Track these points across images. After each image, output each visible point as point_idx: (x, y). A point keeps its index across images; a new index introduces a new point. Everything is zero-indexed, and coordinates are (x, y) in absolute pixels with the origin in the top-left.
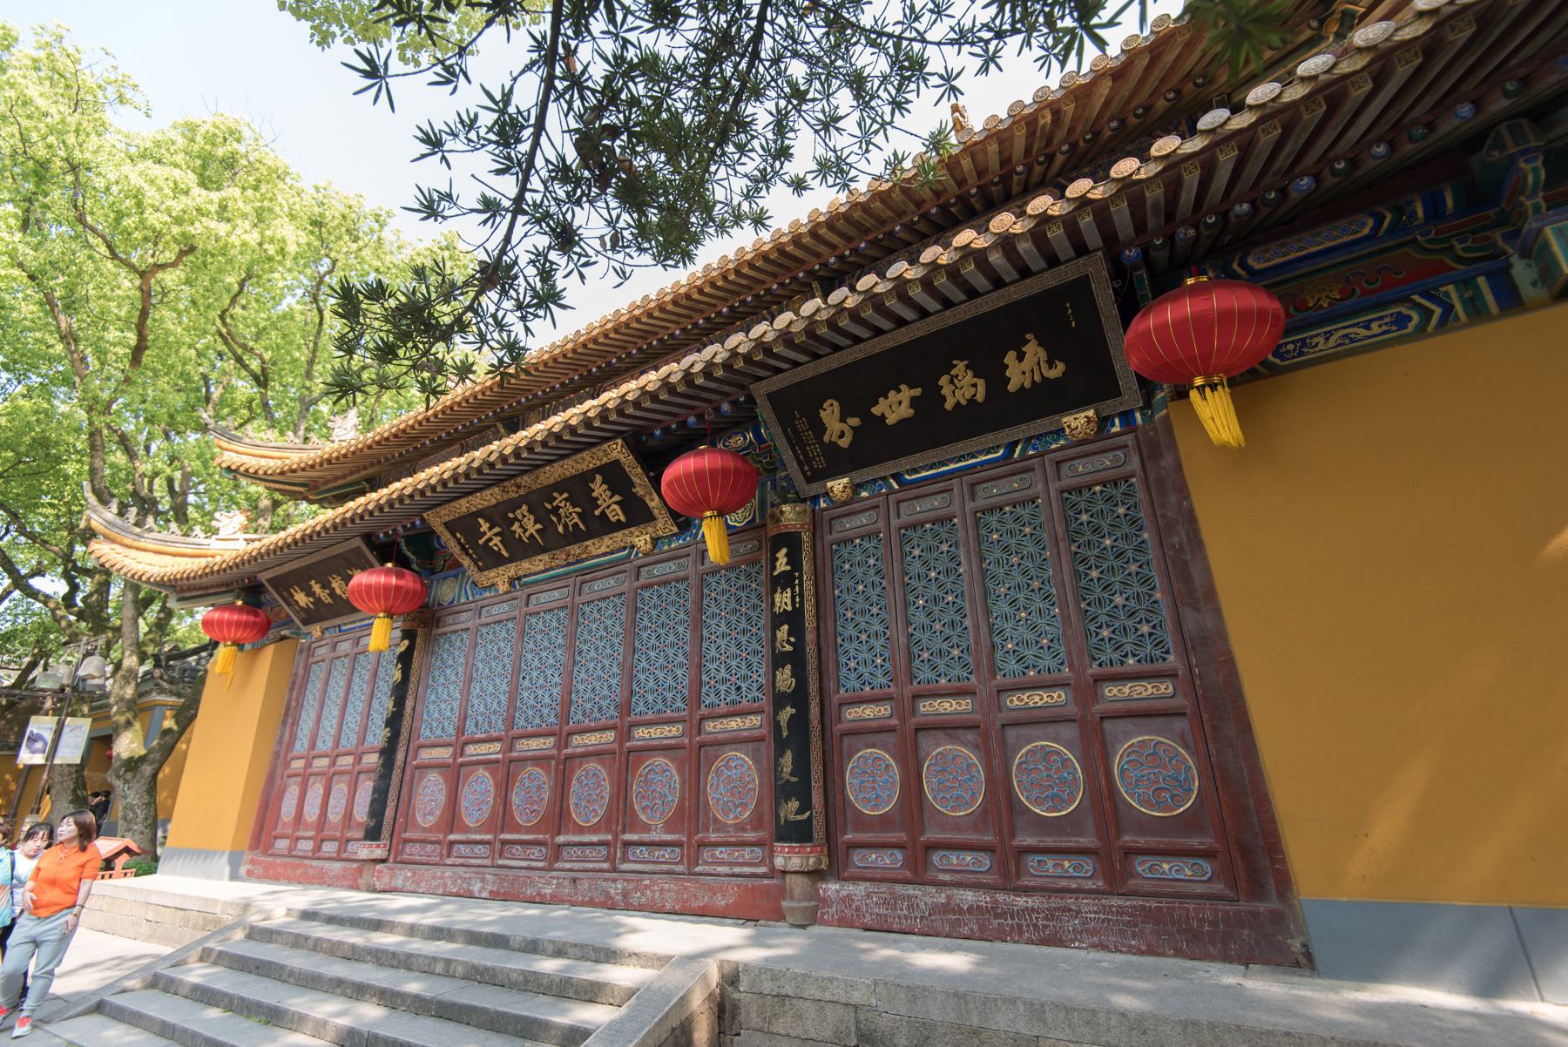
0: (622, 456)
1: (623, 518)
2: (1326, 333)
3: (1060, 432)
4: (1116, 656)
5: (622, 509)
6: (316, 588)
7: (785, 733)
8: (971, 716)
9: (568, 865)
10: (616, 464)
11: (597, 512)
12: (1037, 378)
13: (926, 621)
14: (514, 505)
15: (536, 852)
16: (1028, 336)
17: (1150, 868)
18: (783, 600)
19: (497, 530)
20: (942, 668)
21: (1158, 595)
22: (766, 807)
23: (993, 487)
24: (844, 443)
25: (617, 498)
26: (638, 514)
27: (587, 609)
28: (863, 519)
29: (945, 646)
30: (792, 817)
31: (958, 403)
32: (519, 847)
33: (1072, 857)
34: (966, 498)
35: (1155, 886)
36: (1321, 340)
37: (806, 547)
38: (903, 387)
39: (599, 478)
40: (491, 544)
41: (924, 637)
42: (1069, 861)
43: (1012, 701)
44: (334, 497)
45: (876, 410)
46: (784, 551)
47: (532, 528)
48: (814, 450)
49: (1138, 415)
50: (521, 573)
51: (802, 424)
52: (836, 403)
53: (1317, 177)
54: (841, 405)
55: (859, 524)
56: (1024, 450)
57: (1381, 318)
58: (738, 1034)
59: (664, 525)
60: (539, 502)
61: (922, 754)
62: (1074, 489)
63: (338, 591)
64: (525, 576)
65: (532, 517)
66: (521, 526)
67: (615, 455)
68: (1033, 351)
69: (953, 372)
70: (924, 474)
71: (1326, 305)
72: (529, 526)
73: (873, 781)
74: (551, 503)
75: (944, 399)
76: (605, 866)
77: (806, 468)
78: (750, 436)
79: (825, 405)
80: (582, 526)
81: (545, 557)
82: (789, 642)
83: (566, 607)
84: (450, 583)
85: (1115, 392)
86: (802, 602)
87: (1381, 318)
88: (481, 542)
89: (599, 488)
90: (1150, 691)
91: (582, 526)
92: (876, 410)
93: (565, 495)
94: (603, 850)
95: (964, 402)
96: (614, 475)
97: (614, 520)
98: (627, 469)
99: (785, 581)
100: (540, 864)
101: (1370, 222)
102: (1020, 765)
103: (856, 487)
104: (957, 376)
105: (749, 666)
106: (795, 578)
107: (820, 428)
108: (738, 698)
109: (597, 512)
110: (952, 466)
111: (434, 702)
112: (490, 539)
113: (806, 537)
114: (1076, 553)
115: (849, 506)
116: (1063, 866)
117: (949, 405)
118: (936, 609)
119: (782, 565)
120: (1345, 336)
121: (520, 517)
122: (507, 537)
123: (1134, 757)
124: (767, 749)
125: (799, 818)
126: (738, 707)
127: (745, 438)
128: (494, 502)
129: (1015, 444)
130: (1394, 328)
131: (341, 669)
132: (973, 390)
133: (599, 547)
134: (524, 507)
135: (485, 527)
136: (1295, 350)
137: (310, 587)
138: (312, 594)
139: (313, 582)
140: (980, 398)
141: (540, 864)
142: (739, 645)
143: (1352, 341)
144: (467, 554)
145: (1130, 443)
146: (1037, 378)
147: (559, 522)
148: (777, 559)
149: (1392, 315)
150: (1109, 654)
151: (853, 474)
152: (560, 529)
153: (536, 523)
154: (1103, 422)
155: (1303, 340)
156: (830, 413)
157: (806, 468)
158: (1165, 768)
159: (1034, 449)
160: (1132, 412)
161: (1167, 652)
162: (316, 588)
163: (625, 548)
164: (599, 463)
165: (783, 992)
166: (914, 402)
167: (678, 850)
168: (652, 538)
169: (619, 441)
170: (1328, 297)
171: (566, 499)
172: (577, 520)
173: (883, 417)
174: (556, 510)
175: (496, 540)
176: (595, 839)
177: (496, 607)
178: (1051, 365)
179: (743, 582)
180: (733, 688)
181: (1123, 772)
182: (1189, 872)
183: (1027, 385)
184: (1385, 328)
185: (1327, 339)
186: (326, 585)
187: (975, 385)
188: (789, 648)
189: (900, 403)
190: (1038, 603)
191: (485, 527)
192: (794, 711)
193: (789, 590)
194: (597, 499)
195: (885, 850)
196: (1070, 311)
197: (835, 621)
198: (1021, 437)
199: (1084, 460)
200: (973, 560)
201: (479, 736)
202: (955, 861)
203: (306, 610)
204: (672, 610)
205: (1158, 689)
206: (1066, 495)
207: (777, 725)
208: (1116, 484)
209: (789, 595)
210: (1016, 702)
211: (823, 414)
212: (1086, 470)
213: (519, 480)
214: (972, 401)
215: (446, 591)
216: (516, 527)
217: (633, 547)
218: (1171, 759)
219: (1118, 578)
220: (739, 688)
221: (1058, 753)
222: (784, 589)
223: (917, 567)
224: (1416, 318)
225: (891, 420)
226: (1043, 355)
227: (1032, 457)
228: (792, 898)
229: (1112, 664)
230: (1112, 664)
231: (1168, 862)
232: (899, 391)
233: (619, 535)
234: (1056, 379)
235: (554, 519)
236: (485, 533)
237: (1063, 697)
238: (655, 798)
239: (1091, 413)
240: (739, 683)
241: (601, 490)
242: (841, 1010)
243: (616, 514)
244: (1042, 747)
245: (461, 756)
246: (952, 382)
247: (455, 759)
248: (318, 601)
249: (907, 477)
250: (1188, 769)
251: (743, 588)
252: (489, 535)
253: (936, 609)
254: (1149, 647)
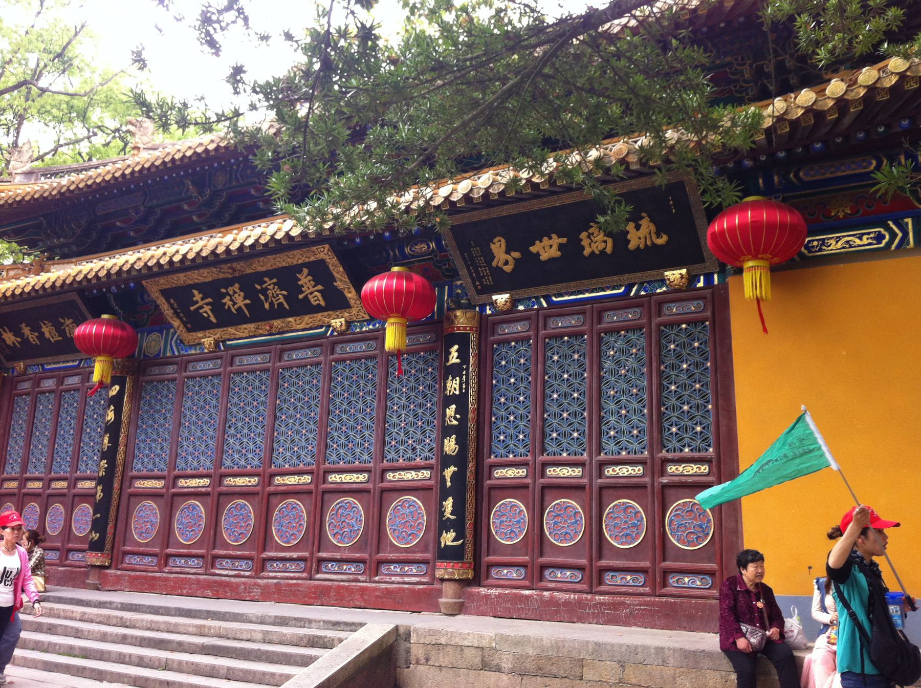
0: (327, 257)
1: (322, 303)
2: (837, 237)
3: (663, 281)
4: (678, 445)
5: (323, 296)
6: (26, 331)
7: (449, 484)
8: (581, 480)
9: (271, 574)
10: (322, 262)
11: (301, 297)
12: (649, 243)
13: (557, 410)
14: (228, 283)
15: (243, 564)
16: (643, 214)
17: (678, 580)
18: (453, 386)
19: (209, 300)
20: (565, 445)
21: (710, 407)
22: (432, 535)
23: (614, 315)
24: (508, 269)
25: (320, 287)
26: (336, 302)
27: (287, 374)
28: (519, 327)
29: (568, 429)
30: (449, 543)
31: (593, 252)
32: (229, 561)
33: (632, 573)
34: (595, 321)
35: (677, 591)
36: (833, 242)
37: (473, 345)
38: (554, 236)
39: (305, 271)
40: (201, 311)
41: (555, 422)
42: (631, 576)
43: (608, 471)
44: (13, 230)
45: (533, 249)
46: (456, 347)
47: (241, 301)
48: (484, 271)
49: (716, 276)
50: (225, 337)
51: (476, 251)
52: (503, 240)
53: (825, 142)
54: (506, 242)
55: (515, 330)
56: (638, 291)
57: (869, 234)
58: (409, 667)
59: (357, 311)
60: (249, 284)
61: (546, 504)
62: (669, 325)
63: (47, 335)
64: (229, 340)
65: (242, 294)
66: (231, 300)
67: (321, 256)
68: (647, 225)
69: (590, 231)
70: (566, 298)
71: (841, 217)
72: (237, 300)
73: (510, 521)
74: (261, 285)
75: (583, 248)
76: (304, 575)
77: (477, 283)
78: (433, 245)
79: (495, 240)
80: (286, 306)
81: (251, 326)
82: (455, 418)
83: (268, 370)
84: (154, 336)
85: (702, 260)
86: (467, 389)
87: (869, 234)
88: (192, 308)
89: (305, 280)
90: (694, 471)
91: (286, 306)
92: (533, 249)
93: (275, 280)
94: (302, 565)
95: (597, 252)
96: (319, 272)
97: (315, 303)
98: (331, 268)
99: (455, 371)
100: (247, 574)
101: (874, 163)
102: (609, 514)
103: (514, 302)
104: (593, 234)
105: (423, 432)
106: (463, 369)
107: (490, 256)
108: (414, 456)
109: (301, 297)
110: (587, 295)
111: (144, 441)
112: (202, 307)
113: (472, 337)
114: (664, 372)
115: (509, 315)
116: (626, 579)
117: (587, 252)
118: (565, 402)
119: (454, 358)
120: (848, 242)
121: (231, 293)
122: (218, 307)
123: (678, 512)
124: (434, 495)
125: (455, 543)
126: (413, 463)
127: (429, 247)
128: (210, 279)
129: (633, 285)
130: (875, 242)
131: (46, 406)
132: (603, 245)
133: (299, 326)
134: (237, 285)
135: (197, 296)
136: (817, 246)
137: (21, 329)
138: (21, 335)
139: (23, 325)
140: (609, 250)
141: (247, 574)
142: (416, 415)
143: (851, 246)
144: (178, 317)
145: (708, 296)
146: (649, 243)
147: (266, 300)
148: (450, 353)
149: (875, 232)
150: (674, 443)
151: (513, 292)
152: (267, 306)
153: (245, 298)
154: (692, 279)
155: (823, 240)
156: (498, 248)
157: (477, 283)
158: (696, 520)
159: (645, 291)
160: (712, 274)
161: (709, 446)
162: (26, 331)
163: (321, 327)
164: (307, 260)
165: (439, 642)
166: (561, 247)
167: (362, 565)
168: (346, 321)
169: (327, 246)
170: (843, 211)
171: (275, 284)
172: (282, 300)
173: (538, 254)
174: (264, 291)
175: (207, 308)
176: (295, 555)
177: (201, 364)
178: (658, 236)
179: (421, 365)
180: (410, 448)
181: (671, 522)
182: (698, 583)
183: (642, 246)
184: (870, 241)
185: (837, 242)
186: (36, 328)
187: (605, 242)
188: (455, 423)
189: (551, 246)
190: (635, 405)
191: (197, 296)
192: (456, 469)
193: (458, 378)
194: (302, 286)
195: (513, 568)
196: (671, 203)
197: (492, 404)
198: (637, 281)
199: (678, 304)
200: (538, 411)
201: (189, 471)
202: (559, 575)
203: (13, 348)
204: (362, 383)
205: (700, 468)
206: (662, 328)
207: (443, 479)
208: (696, 325)
209: (458, 382)
210: (611, 472)
211: (492, 246)
212: (678, 312)
213: (235, 265)
214: (603, 252)
215: (152, 343)
216: (226, 300)
217: (329, 326)
218: (700, 515)
219: (687, 393)
220: (414, 449)
221: (633, 508)
222: (454, 378)
223: (555, 370)
224: (887, 237)
225: (544, 257)
226: (653, 228)
227: (643, 296)
228: (447, 597)
229: (635, 453)
230: (635, 453)
231: (688, 577)
232: (550, 238)
233: (319, 316)
234: (662, 246)
235: (262, 298)
236: (197, 302)
237: (641, 471)
238: (344, 527)
239: (684, 271)
240: (415, 445)
241: (306, 280)
242: (473, 651)
243: (317, 299)
244: (624, 503)
245: (173, 487)
246: (589, 237)
247: (168, 489)
248: (25, 341)
249: (554, 299)
250: (709, 521)
251: (421, 370)
252: (200, 303)
253: (565, 402)
254: (699, 441)
